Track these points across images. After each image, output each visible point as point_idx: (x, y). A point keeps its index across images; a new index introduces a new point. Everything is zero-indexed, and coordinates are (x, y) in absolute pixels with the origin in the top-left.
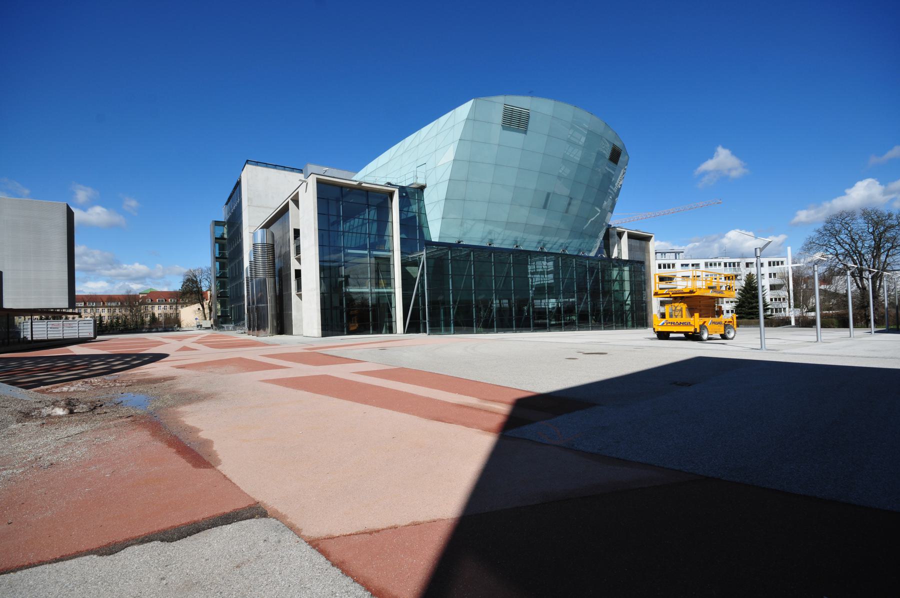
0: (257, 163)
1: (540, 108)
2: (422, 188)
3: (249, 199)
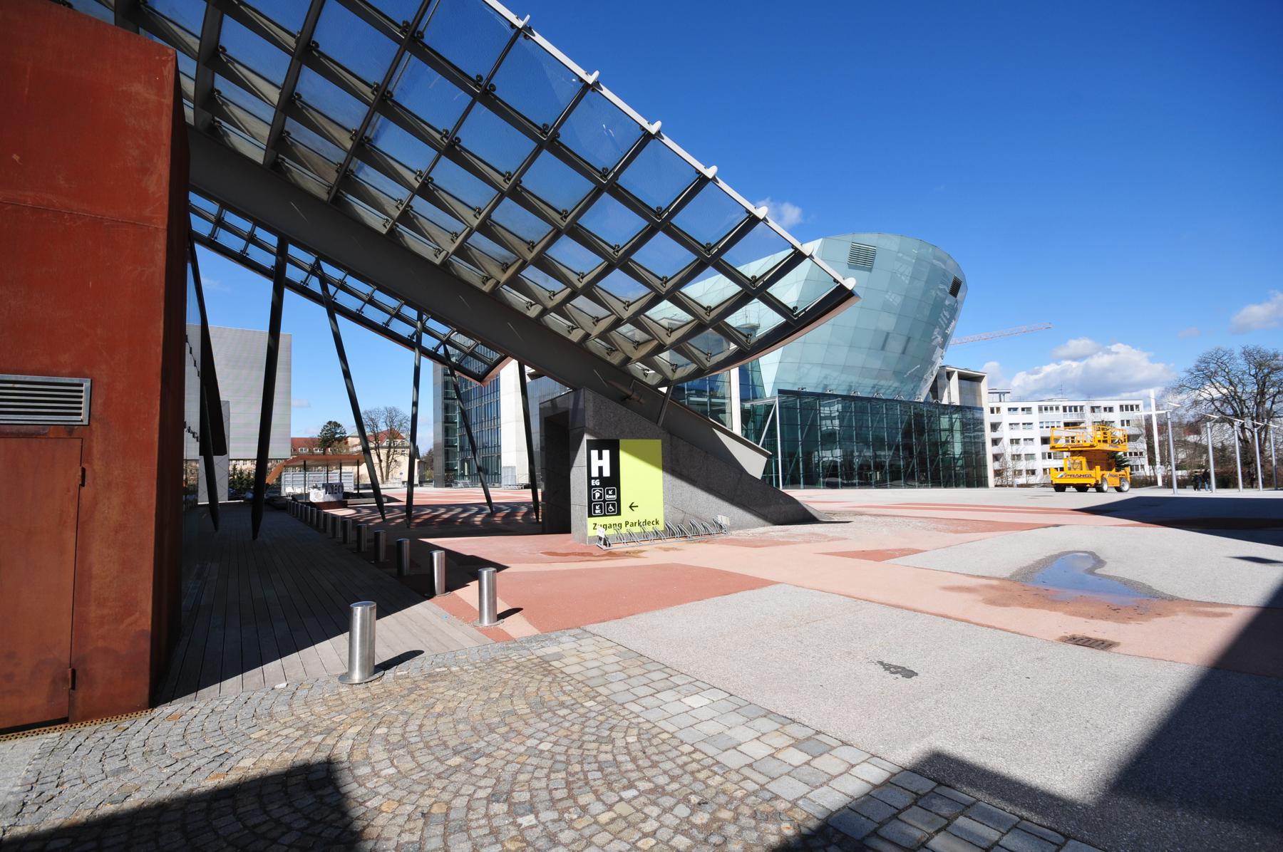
1: (884, 243)
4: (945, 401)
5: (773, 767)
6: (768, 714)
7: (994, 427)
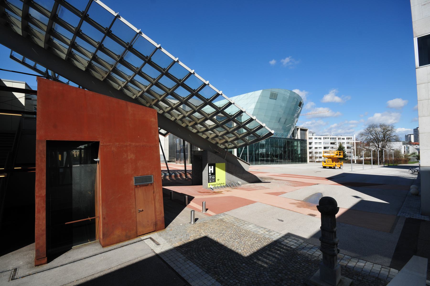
4: (296, 138)
5: (264, 234)
6: (262, 228)
7: (310, 143)
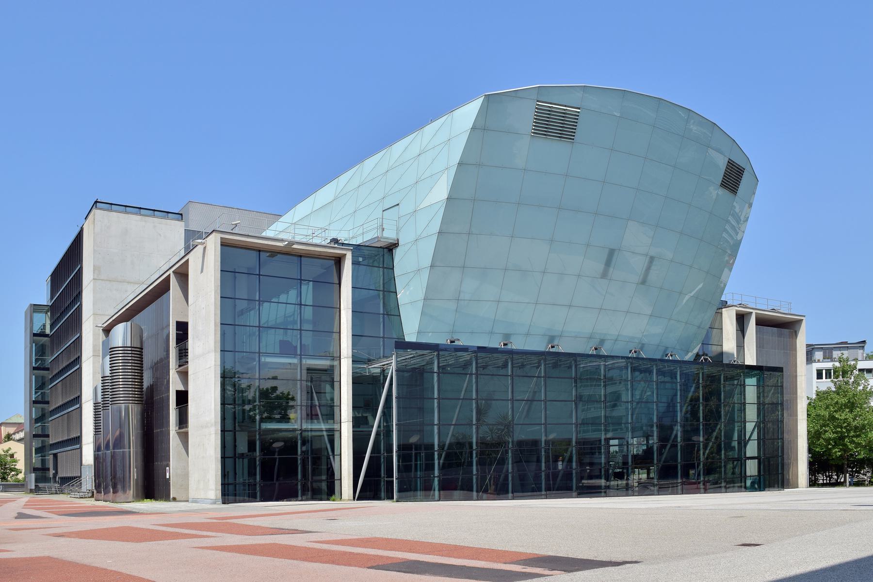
0: (111, 206)
2: (391, 248)
3: (96, 269)
